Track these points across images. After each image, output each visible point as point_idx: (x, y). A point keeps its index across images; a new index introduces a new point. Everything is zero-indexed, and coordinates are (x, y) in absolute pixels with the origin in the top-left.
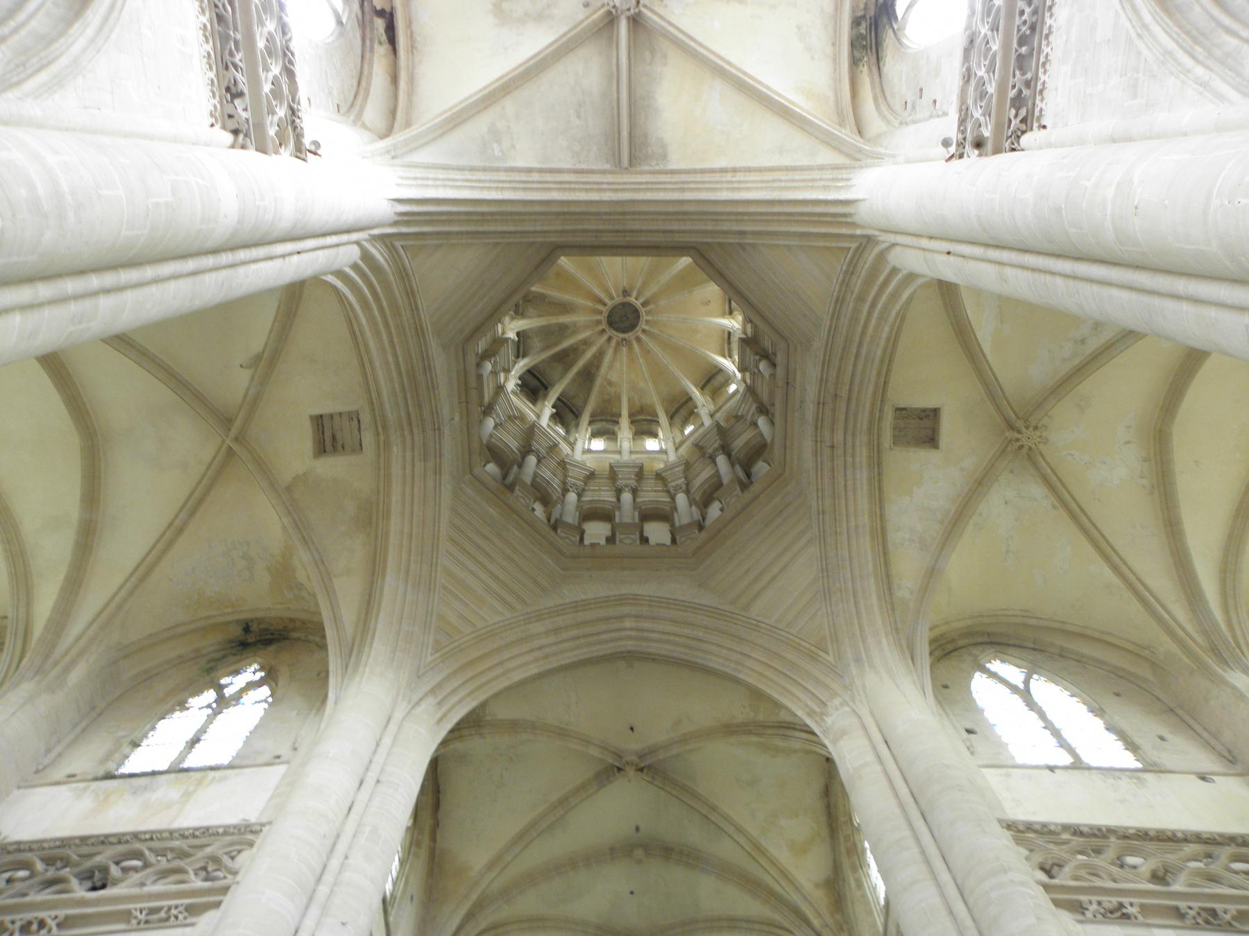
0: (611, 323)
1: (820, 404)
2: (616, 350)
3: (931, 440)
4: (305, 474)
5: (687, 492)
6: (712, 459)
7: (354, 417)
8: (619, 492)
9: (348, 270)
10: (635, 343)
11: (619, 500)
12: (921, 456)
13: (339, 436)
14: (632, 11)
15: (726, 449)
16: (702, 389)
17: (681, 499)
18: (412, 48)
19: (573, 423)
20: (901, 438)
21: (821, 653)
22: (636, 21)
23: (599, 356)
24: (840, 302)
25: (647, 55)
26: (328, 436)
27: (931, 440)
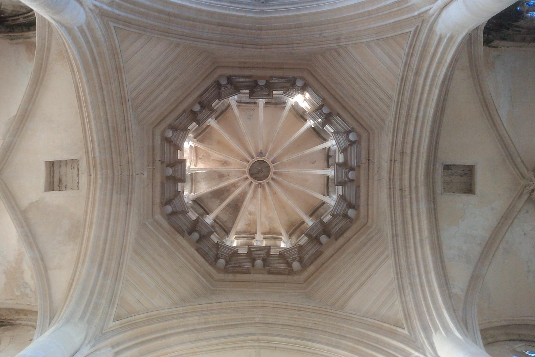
0: (252, 174)
1: (392, 161)
2: (255, 191)
3: (469, 189)
4: (37, 201)
7: (74, 163)
9: (75, 28)
10: (267, 187)
12: (463, 200)
13: (64, 179)
20: (448, 188)
21: (399, 329)
23: (243, 195)
24: (404, 80)
26: (55, 176)
27: (469, 189)
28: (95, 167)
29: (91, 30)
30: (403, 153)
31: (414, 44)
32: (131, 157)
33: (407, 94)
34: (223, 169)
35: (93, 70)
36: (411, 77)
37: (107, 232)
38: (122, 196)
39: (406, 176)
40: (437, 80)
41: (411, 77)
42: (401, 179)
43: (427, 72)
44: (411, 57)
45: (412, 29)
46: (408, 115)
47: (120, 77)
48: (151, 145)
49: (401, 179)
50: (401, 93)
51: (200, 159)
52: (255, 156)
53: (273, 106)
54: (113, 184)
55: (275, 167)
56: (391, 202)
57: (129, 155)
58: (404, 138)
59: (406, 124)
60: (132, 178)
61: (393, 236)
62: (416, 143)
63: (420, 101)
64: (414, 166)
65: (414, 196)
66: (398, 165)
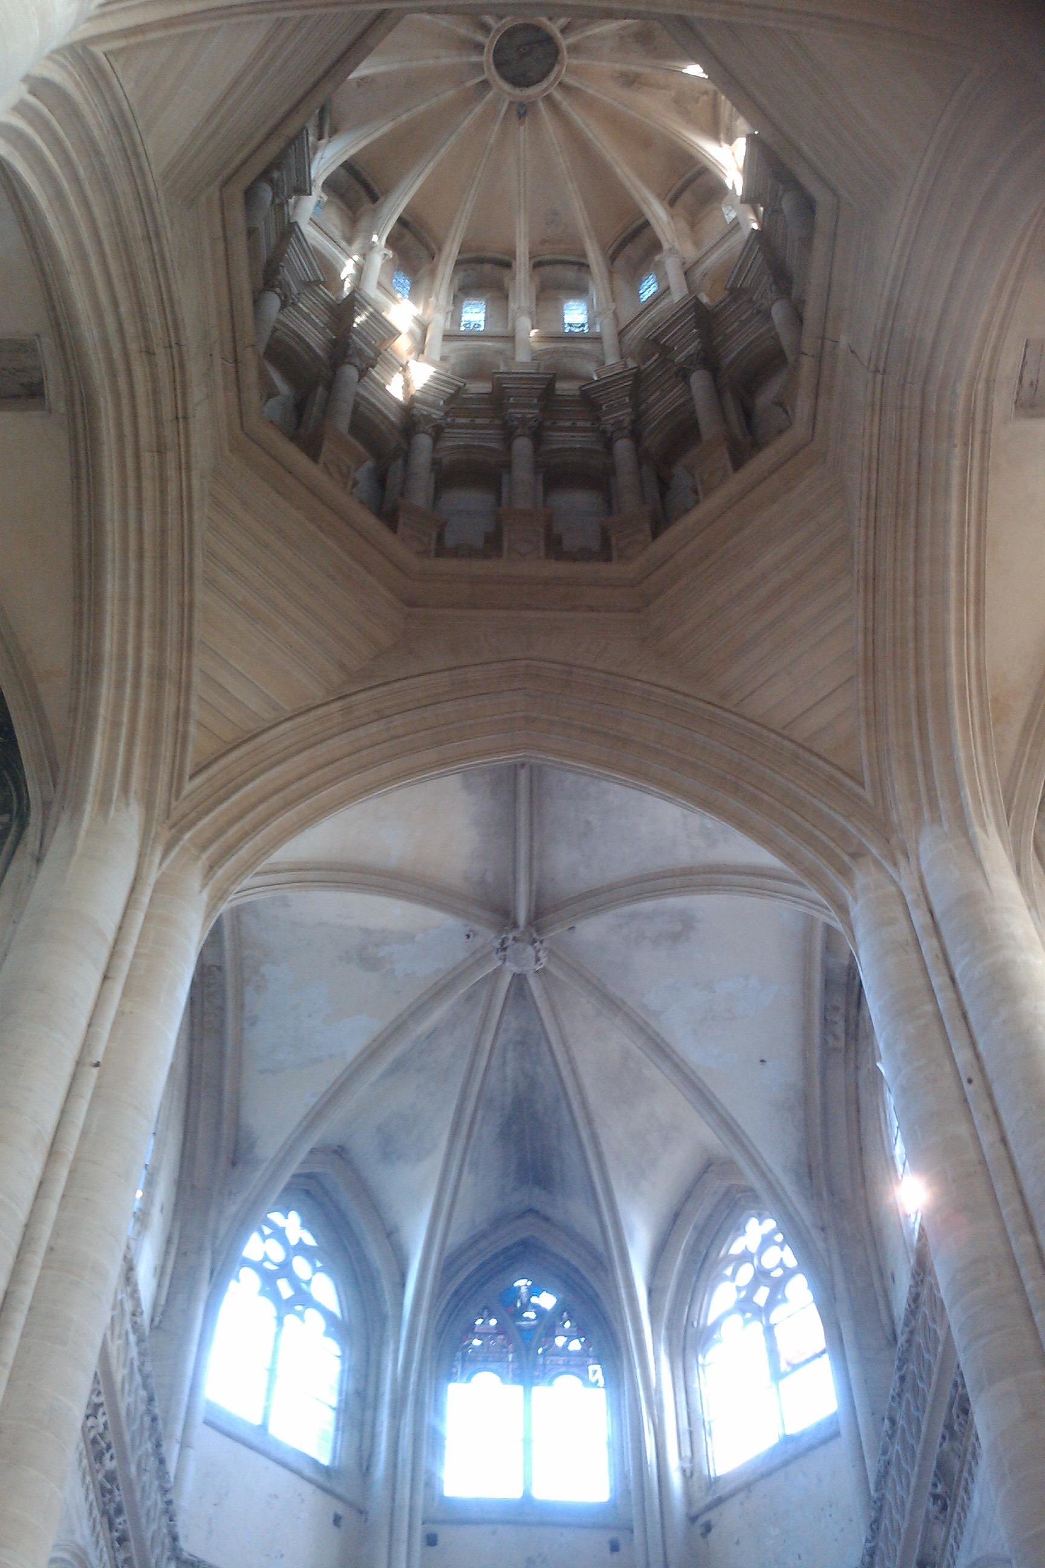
1: (182, 417)
5: (636, 436)
6: (684, 374)
8: (508, 435)
9: (946, 825)
11: (509, 448)
14: (511, 936)
15: (709, 360)
16: (672, 203)
17: (623, 447)
18: (805, 1099)
22: (503, 915)
24: (186, 645)
25: (490, 878)
28: (970, 419)
29: (914, 795)
30: (160, 450)
31: (179, 745)
33: (173, 610)
35: (928, 687)
42: (154, 379)
43: (137, 686)
44: (178, 709)
45: (188, 787)
46: (163, 557)
47: (870, 647)
50: (187, 609)
52: (542, 106)
53: (488, 254)
55: (478, 68)
56: (173, 312)
58: (163, 492)
59: (164, 531)
61: (157, 235)
62: (131, 483)
63: (140, 603)
64: (128, 429)
65: (116, 347)
66: (167, 412)
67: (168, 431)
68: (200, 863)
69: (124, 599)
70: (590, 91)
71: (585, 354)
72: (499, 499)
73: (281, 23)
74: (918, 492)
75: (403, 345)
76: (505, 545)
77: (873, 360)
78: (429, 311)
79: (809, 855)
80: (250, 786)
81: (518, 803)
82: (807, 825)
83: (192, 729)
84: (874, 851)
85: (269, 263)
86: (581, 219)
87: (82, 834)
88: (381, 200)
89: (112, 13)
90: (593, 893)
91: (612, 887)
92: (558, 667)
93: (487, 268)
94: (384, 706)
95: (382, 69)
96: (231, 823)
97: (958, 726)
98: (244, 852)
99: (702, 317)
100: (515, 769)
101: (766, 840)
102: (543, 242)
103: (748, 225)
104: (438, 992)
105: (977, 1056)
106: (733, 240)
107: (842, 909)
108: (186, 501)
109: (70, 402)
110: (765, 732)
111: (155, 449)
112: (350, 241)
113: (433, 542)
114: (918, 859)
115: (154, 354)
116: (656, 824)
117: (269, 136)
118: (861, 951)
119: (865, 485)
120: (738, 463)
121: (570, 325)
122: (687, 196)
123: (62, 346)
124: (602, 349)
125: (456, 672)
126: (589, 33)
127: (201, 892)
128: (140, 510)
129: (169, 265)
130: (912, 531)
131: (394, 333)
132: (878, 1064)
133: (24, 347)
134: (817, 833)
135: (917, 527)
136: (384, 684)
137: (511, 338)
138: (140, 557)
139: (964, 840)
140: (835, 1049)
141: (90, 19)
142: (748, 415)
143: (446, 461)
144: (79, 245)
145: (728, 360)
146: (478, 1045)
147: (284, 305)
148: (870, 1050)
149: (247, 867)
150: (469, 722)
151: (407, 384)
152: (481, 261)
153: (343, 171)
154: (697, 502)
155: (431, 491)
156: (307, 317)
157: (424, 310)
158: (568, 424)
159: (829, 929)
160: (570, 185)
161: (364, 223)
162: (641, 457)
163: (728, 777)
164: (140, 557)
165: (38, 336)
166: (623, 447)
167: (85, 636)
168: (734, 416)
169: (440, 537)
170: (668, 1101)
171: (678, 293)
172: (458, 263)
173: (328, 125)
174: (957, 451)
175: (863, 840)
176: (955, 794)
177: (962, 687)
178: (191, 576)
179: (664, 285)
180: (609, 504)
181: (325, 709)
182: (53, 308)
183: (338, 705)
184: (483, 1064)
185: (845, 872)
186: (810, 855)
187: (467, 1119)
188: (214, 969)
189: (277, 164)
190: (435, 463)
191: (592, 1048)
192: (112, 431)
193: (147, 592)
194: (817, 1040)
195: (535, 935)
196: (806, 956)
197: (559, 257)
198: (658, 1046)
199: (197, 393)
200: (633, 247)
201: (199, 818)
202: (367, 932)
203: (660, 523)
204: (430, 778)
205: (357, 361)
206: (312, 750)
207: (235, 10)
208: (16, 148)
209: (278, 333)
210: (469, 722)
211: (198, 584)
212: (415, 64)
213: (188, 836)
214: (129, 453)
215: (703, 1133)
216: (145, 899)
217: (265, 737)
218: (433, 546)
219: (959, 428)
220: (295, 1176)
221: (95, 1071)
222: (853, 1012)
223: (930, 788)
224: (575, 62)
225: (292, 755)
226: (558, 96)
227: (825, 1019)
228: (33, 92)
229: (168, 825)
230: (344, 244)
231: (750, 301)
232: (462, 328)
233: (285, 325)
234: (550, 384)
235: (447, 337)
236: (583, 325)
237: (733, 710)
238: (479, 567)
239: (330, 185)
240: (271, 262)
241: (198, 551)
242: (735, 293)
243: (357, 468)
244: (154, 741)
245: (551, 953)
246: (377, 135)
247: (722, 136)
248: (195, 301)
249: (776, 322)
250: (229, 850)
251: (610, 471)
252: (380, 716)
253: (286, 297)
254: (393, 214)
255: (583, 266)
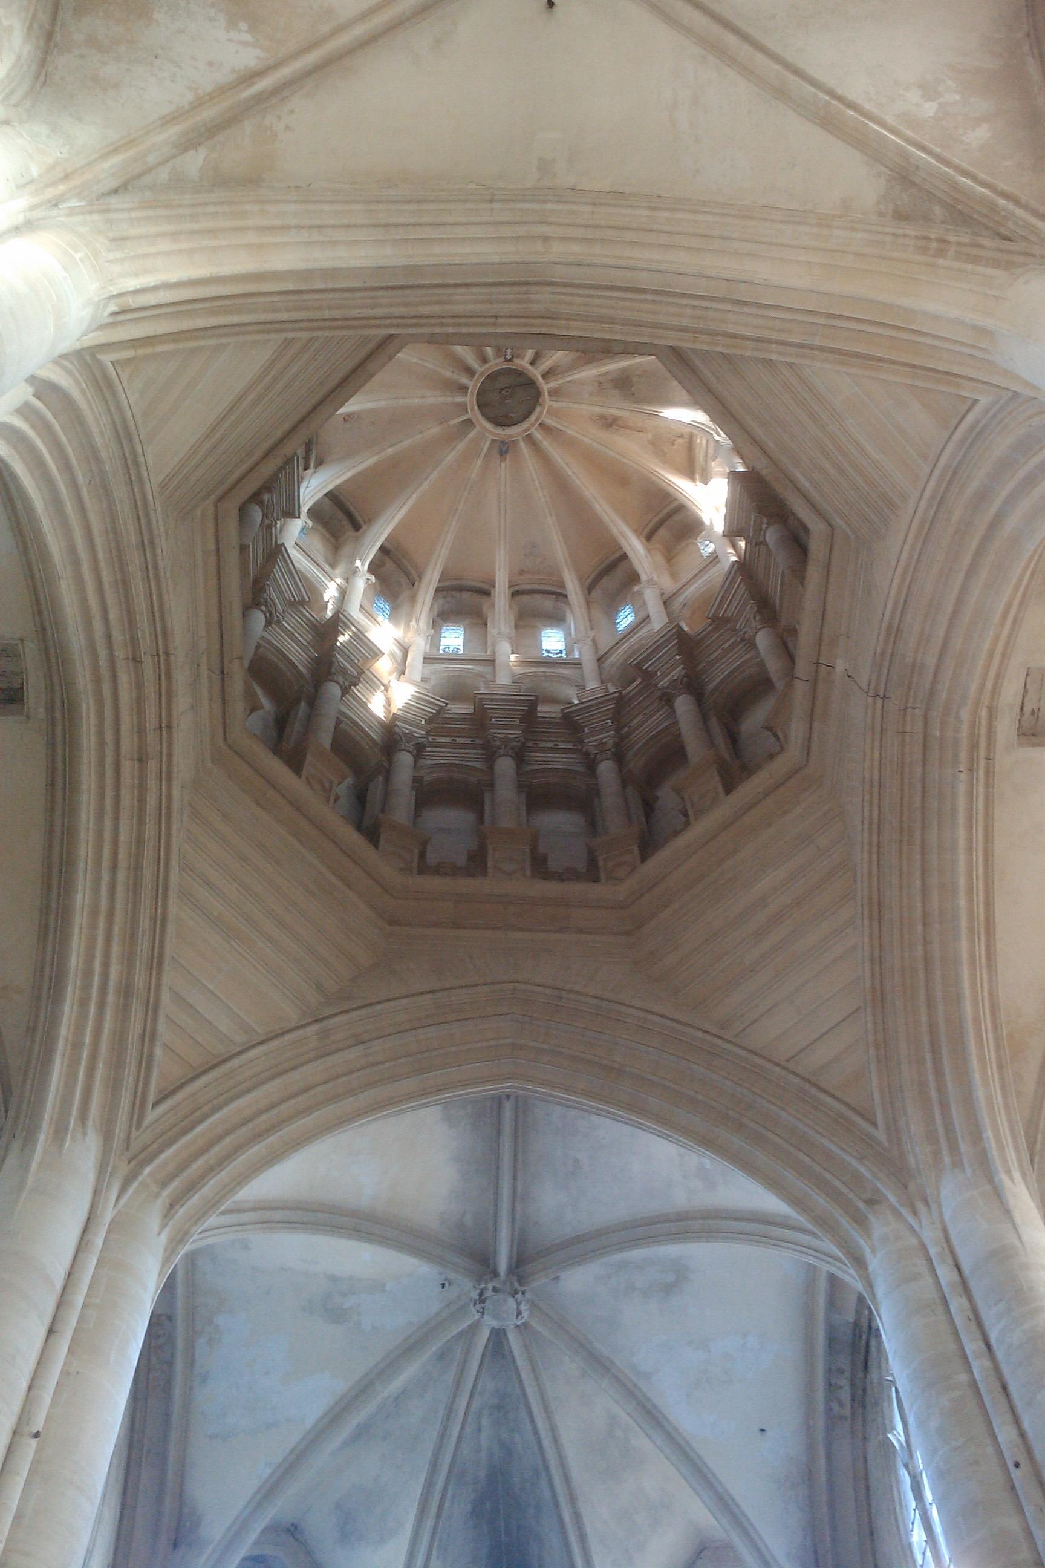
1: (166, 727)
5: (619, 758)
6: (667, 699)
8: (490, 756)
9: (969, 1171)
11: (491, 768)
14: (490, 1286)
15: (693, 685)
16: (649, 538)
17: (606, 769)
18: (809, 1476)
19: (406, 594)
22: (482, 1262)
24: (156, 963)
25: (469, 1220)
28: (974, 747)
29: (931, 1137)
32: (872, 748)
33: (145, 923)
34: (618, 408)
35: (941, 1024)
36: (140, 978)
37: (964, 590)
38: (909, 660)
39: (126, 696)
40: (77, 992)
41: (140, 978)
42: (139, 685)
43: (102, 1005)
44: (144, 1031)
45: (151, 1116)
48: (816, 725)
49: (139, 685)
50: (160, 922)
51: (681, 436)
52: (524, 448)
54: (932, 693)
55: (463, 408)
56: (163, 621)
57: (877, 755)
58: (142, 801)
59: (140, 841)
60: (876, 689)
61: (152, 543)
62: (109, 794)
64: (109, 737)
65: (103, 653)
66: (151, 721)
67: (151, 738)
68: (159, 1202)
69: (94, 912)
70: (570, 432)
71: (567, 680)
72: (481, 819)
73: (288, 343)
74: (923, 819)
75: (383, 667)
76: (490, 864)
77: (873, 685)
78: (410, 634)
79: (820, 1200)
80: (217, 1116)
81: (502, 1138)
82: (818, 1168)
83: (158, 1052)
84: (892, 1198)
85: (256, 582)
86: (559, 551)
87: (34, 1165)
88: (365, 527)
89: (122, 323)
90: (579, 1239)
91: (601, 1233)
92: (548, 991)
93: (466, 595)
94: (366, 1031)
95: (369, 405)
96: (197, 1155)
97: (975, 1063)
98: (208, 1189)
99: (685, 645)
100: (498, 1101)
101: (773, 1184)
102: (522, 572)
103: (728, 558)
104: (409, 1349)
105: (1022, 1435)
106: (711, 572)
107: (859, 1262)
108: (164, 813)
109: (50, 708)
110: (768, 1065)
111: (136, 757)
112: (333, 566)
113: (416, 859)
114: (940, 1206)
115: (141, 662)
116: (649, 1164)
117: (266, 455)
118: (883, 1310)
119: (867, 809)
120: (728, 789)
121: (548, 652)
122: (663, 532)
123: (46, 651)
124: (582, 675)
125: (439, 995)
126: (570, 379)
127: (159, 1234)
128: (116, 818)
129: (162, 575)
130: (918, 857)
131: (376, 653)
132: (890, 1436)
133: (8, 652)
134: (827, 1175)
135: (923, 854)
136: (365, 1006)
137: (492, 662)
138: (114, 868)
139: (988, 1187)
140: (842, 1418)
141: (102, 327)
142: (733, 738)
143: (427, 779)
144: (72, 550)
145: (710, 687)
146: (450, 1409)
147: (268, 623)
148: (880, 1419)
149: (210, 1206)
150: (453, 1049)
151: (389, 703)
152: (461, 589)
153: (327, 500)
154: (687, 824)
155: (413, 807)
156: (291, 635)
157: (405, 632)
158: (550, 745)
159: (833, 1280)
160: (549, 519)
161: (346, 550)
162: (625, 780)
163: (731, 1113)
164: (114, 868)
165: (21, 640)
166: (606, 769)
167: (49, 950)
168: (720, 740)
169: (422, 855)
170: (657, 1474)
171: (658, 622)
172: (438, 590)
173: (312, 455)
174: (963, 776)
175: (879, 1185)
176: (977, 1136)
177: (977, 1021)
178: (166, 889)
179: (642, 615)
180: (593, 825)
181: (301, 1032)
182: (40, 612)
183: (316, 1027)
184: (455, 1432)
185: (860, 1220)
186: (821, 1200)
187: (437, 1496)
188: (163, 1318)
189: (268, 486)
190: (417, 781)
191: (576, 1415)
192: (93, 739)
193: (119, 906)
194: (821, 1407)
195: (516, 1285)
196: (809, 1314)
197: (536, 587)
198: (649, 1412)
199: (182, 702)
200: (611, 577)
201: (160, 1151)
202: (333, 1279)
203: (648, 846)
204: (406, 1111)
205: (341, 680)
206: (284, 1078)
207: (243, 329)
208: (15, 448)
209: (262, 650)
210: (453, 1049)
211: (172, 895)
212: (401, 402)
213: (147, 1170)
214: (109, 760)
215: (698, 1512)
216: (99, 1241)
217: (235, 1063)
218: (415, 865)
219: (963, 755)
220: (245, 1559)
221: (34, 1442)
222: (860, 1375)
223: (949, 1129)
224: (555, 405)
225: (263, 1083)
226: (538, 435)
227: (830, 1384)
228: (37, 396)
229: (129, 1157)
230: (327, 568)
231: (734, 630)
232: (441, 652)
233: (269, 643)
234: (533, 705)
235: (428, 659)
236: (561, 652)
237: (734, 1040)
238: (465, 885)
239: (315, 513)
240: (260, 579)
241: (174, 863)
242: (718, 622)
243: (340, 783)
244: (117, 1064)
245: (533, 1306)
246: (361, 468)
247: (697, 477)
248: (185, 612)
249: (761, 651)
250: (192, 1187)
251: (595, 791)
252: (359, 1041)
253: (271, 614)
254: (376, 541)
255: (561, 596)
